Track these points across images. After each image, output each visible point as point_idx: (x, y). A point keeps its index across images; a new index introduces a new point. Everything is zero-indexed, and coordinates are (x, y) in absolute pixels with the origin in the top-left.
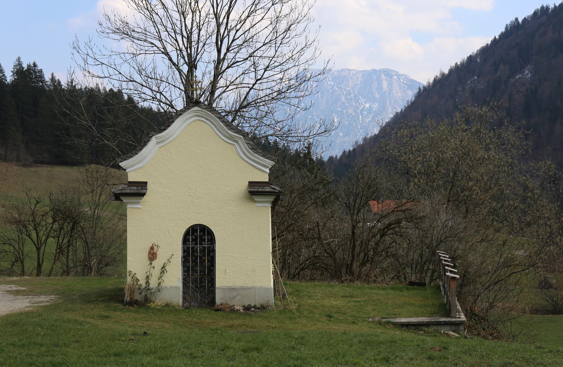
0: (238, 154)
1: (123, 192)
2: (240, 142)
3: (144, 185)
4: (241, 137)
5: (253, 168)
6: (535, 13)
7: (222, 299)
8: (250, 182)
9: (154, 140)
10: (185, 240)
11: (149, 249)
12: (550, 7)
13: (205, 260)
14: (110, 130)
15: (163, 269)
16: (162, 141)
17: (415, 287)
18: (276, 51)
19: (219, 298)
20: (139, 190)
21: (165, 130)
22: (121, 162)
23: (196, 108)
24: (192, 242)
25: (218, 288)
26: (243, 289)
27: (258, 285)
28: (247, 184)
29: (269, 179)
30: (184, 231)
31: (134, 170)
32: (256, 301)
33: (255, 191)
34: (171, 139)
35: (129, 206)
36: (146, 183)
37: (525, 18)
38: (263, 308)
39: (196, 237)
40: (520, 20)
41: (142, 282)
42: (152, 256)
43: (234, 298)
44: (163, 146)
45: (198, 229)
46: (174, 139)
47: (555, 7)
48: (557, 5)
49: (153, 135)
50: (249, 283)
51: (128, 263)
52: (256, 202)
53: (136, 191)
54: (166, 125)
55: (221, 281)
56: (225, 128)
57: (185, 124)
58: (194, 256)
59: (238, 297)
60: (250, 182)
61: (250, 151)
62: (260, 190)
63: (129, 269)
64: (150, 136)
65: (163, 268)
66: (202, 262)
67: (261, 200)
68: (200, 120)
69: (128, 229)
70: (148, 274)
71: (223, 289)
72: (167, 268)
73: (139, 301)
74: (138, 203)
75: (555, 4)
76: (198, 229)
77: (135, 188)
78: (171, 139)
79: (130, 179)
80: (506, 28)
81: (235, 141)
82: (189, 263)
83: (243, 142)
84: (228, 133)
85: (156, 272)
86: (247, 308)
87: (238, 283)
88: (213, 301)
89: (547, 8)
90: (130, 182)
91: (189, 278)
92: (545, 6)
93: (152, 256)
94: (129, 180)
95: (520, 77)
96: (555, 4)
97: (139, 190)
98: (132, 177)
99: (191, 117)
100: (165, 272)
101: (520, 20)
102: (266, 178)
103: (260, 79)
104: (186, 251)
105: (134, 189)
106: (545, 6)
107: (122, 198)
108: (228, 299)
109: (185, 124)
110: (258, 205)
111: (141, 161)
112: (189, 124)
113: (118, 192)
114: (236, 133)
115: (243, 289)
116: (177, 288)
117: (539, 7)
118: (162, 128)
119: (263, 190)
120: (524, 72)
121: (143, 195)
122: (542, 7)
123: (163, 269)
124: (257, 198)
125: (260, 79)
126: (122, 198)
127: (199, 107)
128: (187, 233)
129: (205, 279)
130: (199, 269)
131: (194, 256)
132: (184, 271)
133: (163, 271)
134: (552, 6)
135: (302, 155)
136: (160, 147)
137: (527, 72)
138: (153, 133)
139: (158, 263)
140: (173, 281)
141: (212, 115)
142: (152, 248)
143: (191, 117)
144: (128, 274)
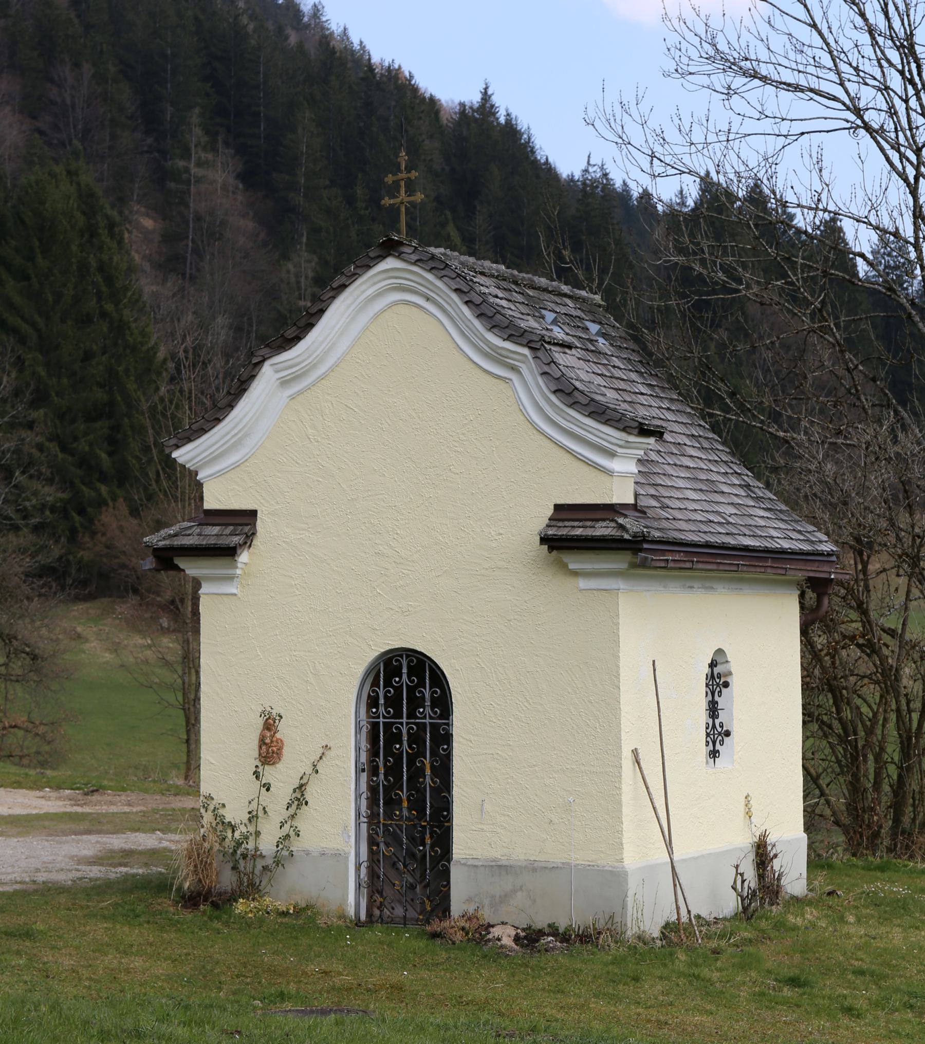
0: (523, 411)
1: (178, 542)
3: (245, 520)
4: (526, 351)
5: (568, 459)
7: (469, 900)
8: (558, 507)
14: (851, 439)
15: (299, 798)
21: (298, 339)
22: (177, 447)
23: (390, 263)
25: (458, 862)
26: (535, 870)
27: (579, 857)
28: (550, 512)
30: (359, 669)
34: (322, 369)
35: (205, 589)
36: (253, 514)
39: (399, 690)
42: (269, 751)
43: (505, 898)
44: (300, 392)
46: (331, 369)
50: (554, 853)
52: (575, 574)
54: (302, 323)
55: (467, 841)
56: (477, 323)
57: (364, 319)
58: (393, 755)
59: (519, 894)
61: (553, 398)
62: (578, 532)
64: (255, 360)
66: (416, 774)
68: (407, 303)
70: (254, 805)
72: (311, 793)
74: (231, 578)
77: (216, 530)
78: (322, 369)
79: (210, 503)
81: (513, 368)
83: (532, 372)
84: (487, 342)
86: (530, 939)
87: (521, 850)
88: (441, 903)
93: (269, 751)
94: (207, 506)
98: (215, 497)
105: (212, 534)
107: (181, 563)
108: (486, 902)
109: (364, 319)
110: (582, 583)
112: (376, 316)
113: (161, 544)
114: (509, 338)
115: (533, 868)
118: (290, 333)
119: (589, 532)
121: (230, 552)
123: (299, 798)
124: (575, 562)
126: (181, 563)
127: (399, 257)
128: (439, 679)
129: (423, 833)
130: (404, 797)
131: (393, 755)
135: (70, 323)
136: (292, 398)
138: (265, 351)
139: (283, 777)
140: (327, 837)
141: (439, 283)
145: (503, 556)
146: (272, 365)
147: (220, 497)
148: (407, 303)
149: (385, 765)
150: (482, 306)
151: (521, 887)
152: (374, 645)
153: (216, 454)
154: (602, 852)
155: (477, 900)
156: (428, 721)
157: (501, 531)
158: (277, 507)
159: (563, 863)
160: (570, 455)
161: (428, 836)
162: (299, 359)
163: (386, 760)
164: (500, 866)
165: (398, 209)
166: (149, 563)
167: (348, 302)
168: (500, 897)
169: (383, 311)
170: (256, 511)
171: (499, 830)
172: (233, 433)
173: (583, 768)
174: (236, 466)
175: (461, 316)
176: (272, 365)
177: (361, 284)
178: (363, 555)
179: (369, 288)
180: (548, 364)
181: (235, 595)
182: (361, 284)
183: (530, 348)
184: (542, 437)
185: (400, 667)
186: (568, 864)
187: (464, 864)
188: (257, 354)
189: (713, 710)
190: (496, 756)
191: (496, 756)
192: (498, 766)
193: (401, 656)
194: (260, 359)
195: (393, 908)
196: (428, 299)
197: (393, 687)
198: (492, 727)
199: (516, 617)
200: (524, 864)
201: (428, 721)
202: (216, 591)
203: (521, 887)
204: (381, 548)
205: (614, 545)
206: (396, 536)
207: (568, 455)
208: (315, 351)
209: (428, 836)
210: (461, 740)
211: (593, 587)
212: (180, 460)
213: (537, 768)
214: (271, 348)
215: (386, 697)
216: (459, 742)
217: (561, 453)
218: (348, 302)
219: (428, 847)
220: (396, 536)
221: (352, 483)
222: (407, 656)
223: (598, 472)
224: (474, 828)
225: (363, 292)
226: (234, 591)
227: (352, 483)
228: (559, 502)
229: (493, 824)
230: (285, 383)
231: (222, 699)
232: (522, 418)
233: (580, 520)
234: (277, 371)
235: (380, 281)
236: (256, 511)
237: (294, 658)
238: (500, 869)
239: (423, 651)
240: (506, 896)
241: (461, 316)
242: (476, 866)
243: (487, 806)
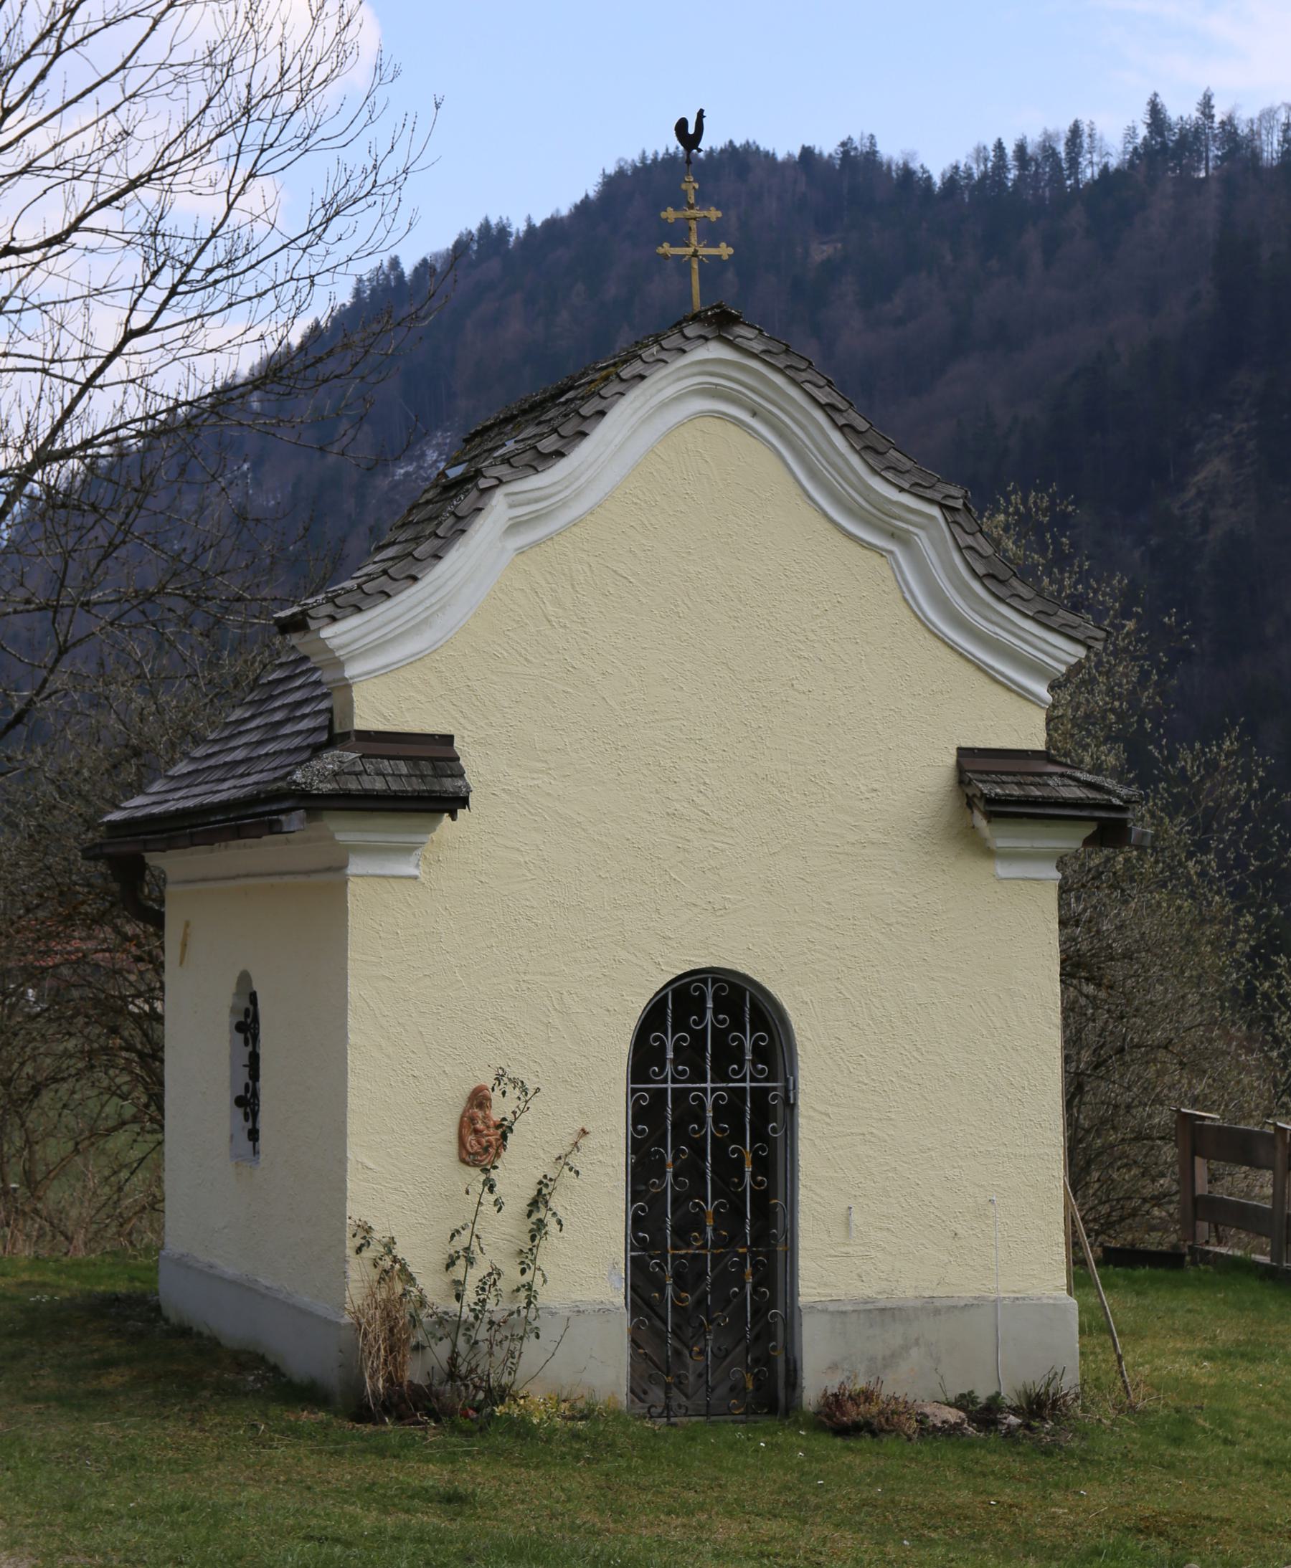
2: (923, 540)
3: (435, 753)
4: (935, 511)
6: (461, 246)
7: (834, 1367)
9: (499, 508)
10: (644, 1058)
11: (460, 1103)
12: (513, 230)
13: (741, 1161)
16: (536, 518)
17: (1142, 1272)
18: (230, 207)
19: (820, 1368)
20: (422, 782)
21: (560, 454)
22: (333, 619)
23: (715, 351)
24: (675, 1062)
26: (937, 1312)
28: (951, 760)
29: (1050, 741)
30: (638, 1005)
31: (388, 670)
32: (1009, 1377)
33: (991, 794)
35: (356, 866)
37: (425, 260)
38: (1039, 1406)
39: (699, 1037)
40: (408, 268)
41: (431, 1285)
42: (480, 1138)
43: (891, 1359)
44: (536, 544)
45: (710, 993)
47: (531, 229)
48: (538, 223)
49: (501, 482)
50: (964, 1284)
51: (353, 1185)
52: (990, 853)
53: (416, 785)
56: (855, 461)
59: (914, 1352)
60: (963, 752)
61: (976, 586)
63: (356, 1210)
64: (483, 483)
65: (534, 1204)
67: (1024, 844)
68: (722, 416)
69: (1058, 988)
71: (838, 1314)
73: (423, 1392)
75: (529, 219)
76: (710, 993)
80: (358, 292)
81: (893, 535)
82: (662, 1175)
84: (867, 492)
85: (500, 1233)
87: (909, 1283)
89: (503, 231)
90: (365, 736)
91: (663, 1257)
92: (494, 221)
93: (480, 1138)
95: (407, 474)
96: (529, 219)
97: (422, 782)
98: (373, 710)
99: (678, 398)
100: (552, 1226)
101: (408, 268)
102: (1035, 739)
103: (144, 331)
104: (644, 1114)
106: (494, 221)
110: (1002, 869)
111: (426, 621)
112: (670, 431)
115: (933, 1309)
116: (604, 1311)
117: (474, 227)
120: (423, 455)
122: (485, 227)
124: (1003, 837)
125: (144, 331)
128: (652, 1019)
129: (742, 1265)
132: (637, 1223)
133: (541, 1223)
134: (518, 226)
136: (521, 551)
137: (432, 455)
142: (479, 1099)
143: (678, 398)
144: (351, 1244)
145: (879, 824)
146: (507, 495)
147: (385, 711)
148: (722, 416)
149: (675, 1159)
150: (868, 434)
151: (917, 1340)
152: (667, 964)
153: (390, 636)
154: (1034, 1276)
155: (846, 1366)
156: (709, 1085)
157: (875, 786)
158: (491, 731)
159: (975, 1298)
160: (980, 675)
161: (749, 1269)
162: (552, 490)
163: (677, 1152)
164: (883, 1310)
165: (689, 263)
166: (1141, 826)
167: (637, 404)
168: (884, 1359)
169: (681, 424)
170: (451, 737)
171: (873, 1253)
172: (428, 603)
173: (1004, 1150)
174: (415, 660)
175: (824, 446)
176: (507, 495)
177: (661, 379)
178: (646, 816)
179: (669, 385)
180: (973, 534)
181: (416, 878)
182: (661, 379)
183: (942, 507)
184: (939, 644)
185: (703, 997)
186: (983, 1298)
187: (825, 1311)
188: (487, 474)
189: (254, 1059)
190: (868, 1137)
191: (868, 1137)
192: (871, 1152)
193: (704, 981)
194: (494, 482)
195: (645, 1393)
196: (754, 414)
197: (691, 1031)
198: (862, 1091)
199: (900, 919)
200: (919, 1303)
201: (748, 1085)
202: (379, 872)
203: (917, 1340)
204: (678, 806)
205: (414, 805)
206: (702, 788)
207: (980, 675)
208: (578, 478)
209: (749, 1269)
210: (812, 1114)
211: (1020, 875)
212: (332, 644)
213: (932, 1153)
214: (512, 466)
215: (677, 1048)
216: (810, 1118)
217: (968, 671)
218: (637, 404)
219: (749, 1288)
220: (702, 788)
221: (625, 698)
222: (714, 981)
223: (1023, 702)
224: (832, 1252)
225: (660, 390)
226: (412, 871)
227: (625, 698)
228: (964, 745)
229: (864, 1244)
230: (515, 526)
231: (389, 1057)
232: (907, 612)
233: (1014, 774)
234: (511, 506)
235: (687, 377)
236: (451, 737)
237: (524, 986)
238: (883, 1314)
239: (688, 968)
240: (893, 1356)
241: (824, 446)
242: (844, 1313)
243: (855, 1217)
